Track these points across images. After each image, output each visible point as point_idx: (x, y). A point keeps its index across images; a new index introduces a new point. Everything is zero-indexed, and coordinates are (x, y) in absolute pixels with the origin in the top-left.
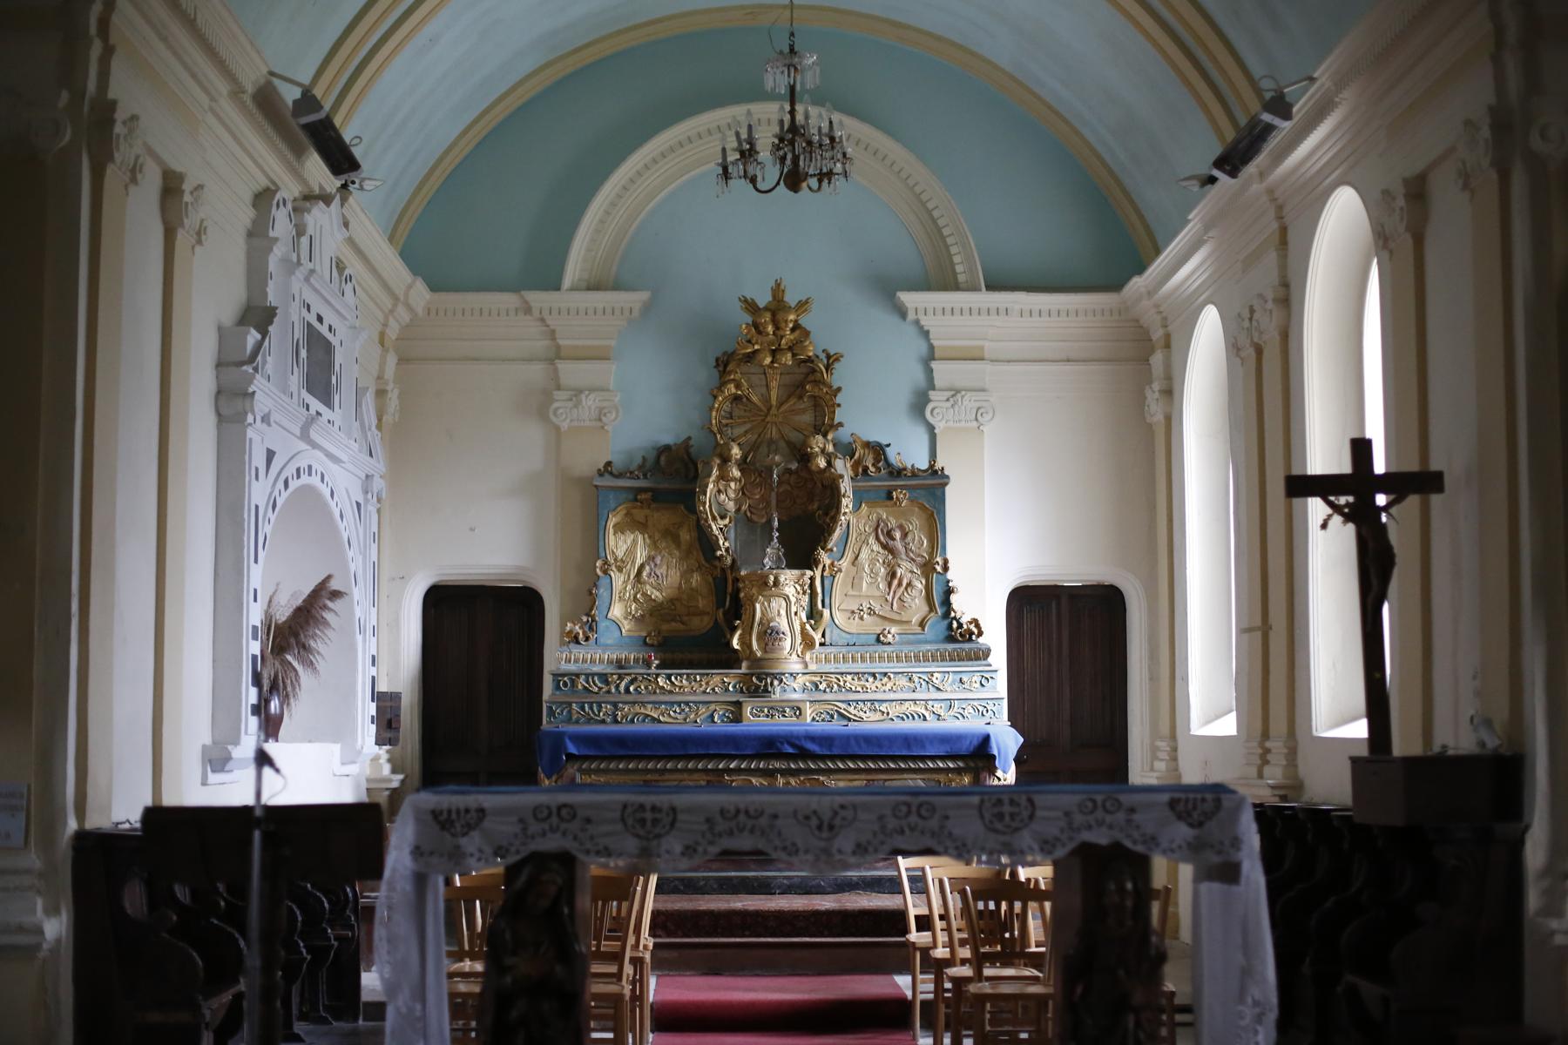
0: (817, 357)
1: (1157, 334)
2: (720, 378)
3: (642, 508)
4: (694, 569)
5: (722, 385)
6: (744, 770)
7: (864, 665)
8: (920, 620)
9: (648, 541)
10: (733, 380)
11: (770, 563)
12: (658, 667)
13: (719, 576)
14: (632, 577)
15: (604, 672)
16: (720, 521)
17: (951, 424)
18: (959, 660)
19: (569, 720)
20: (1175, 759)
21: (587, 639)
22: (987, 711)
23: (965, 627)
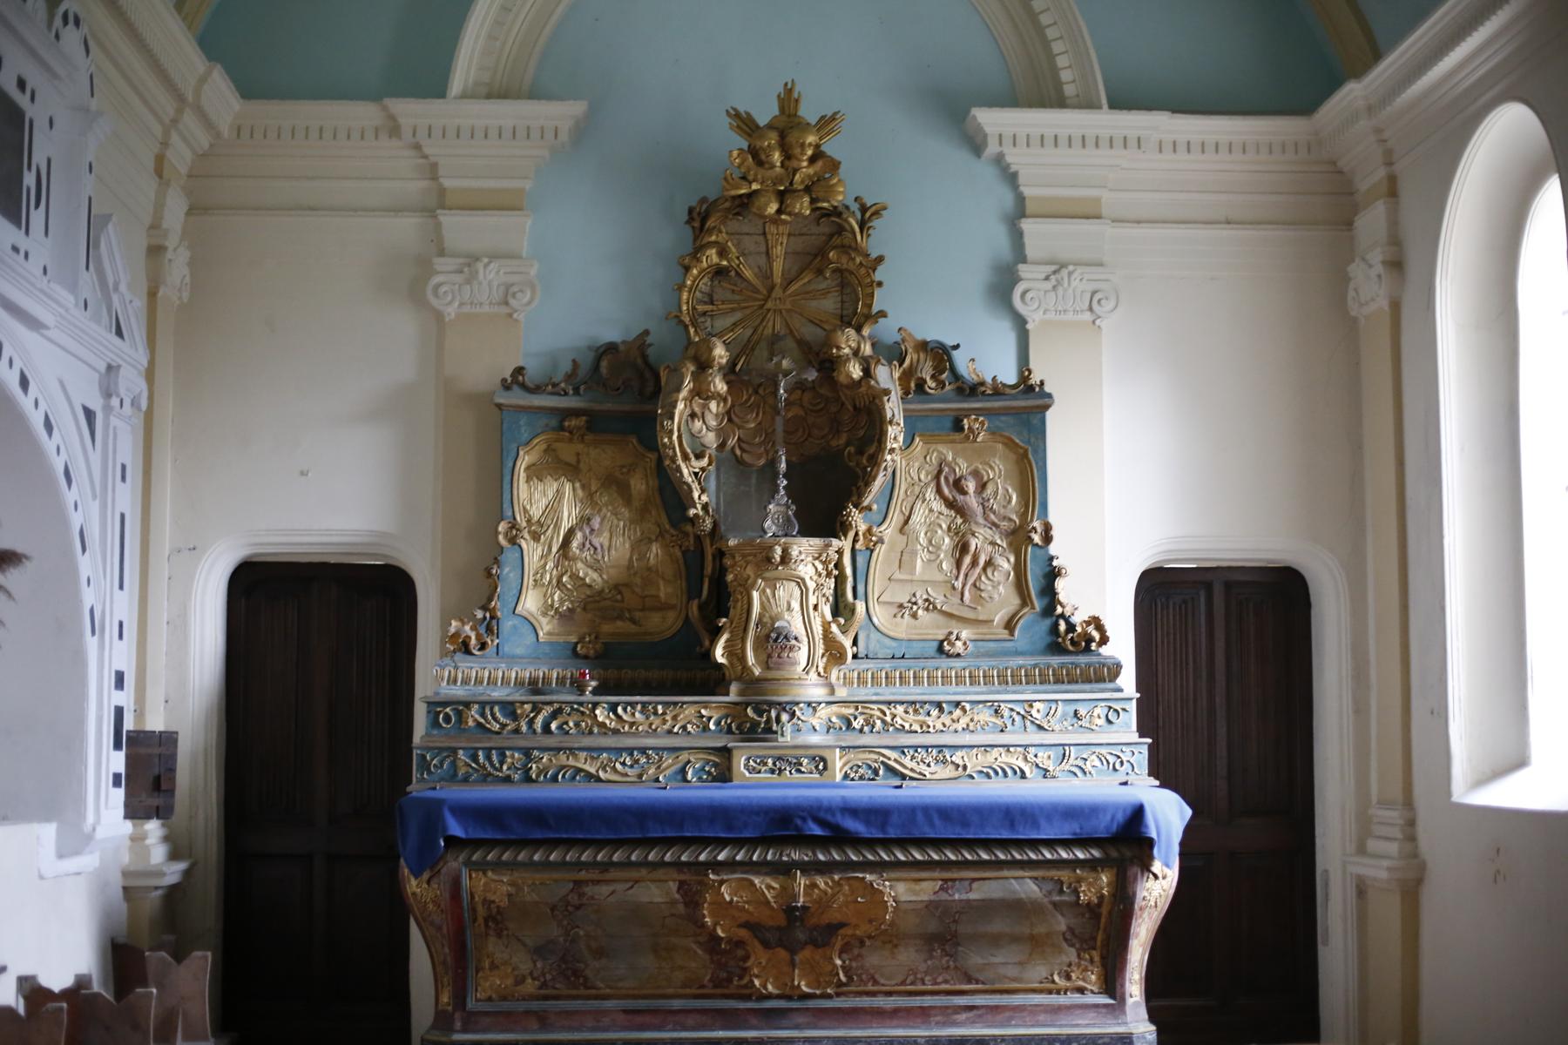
0: (847, 208)
1: (1371, 177)
2: (695, 240)
3: (571, 440)
4: (653, 537)
5: (697, 251)
6: (741, 863)
7: (918, 690)
8: (1006, 618)
9: (580, 493)
10: (716, 243)
11: (774, 528)
12: (595, 692)
13: (692, 548)
14: (554, 550)
15: (510, 698)
16: (694, 462)
17: (1051, 316)
18: (1069, 682)
19: (452, 777)
20: (1411, 838)
21: (483, 646)
22: (1122, 763)
23: (1079, 629)
